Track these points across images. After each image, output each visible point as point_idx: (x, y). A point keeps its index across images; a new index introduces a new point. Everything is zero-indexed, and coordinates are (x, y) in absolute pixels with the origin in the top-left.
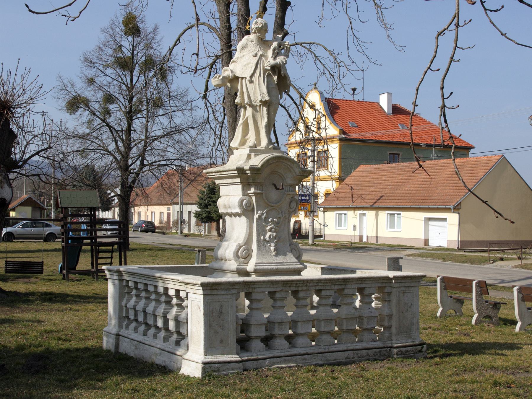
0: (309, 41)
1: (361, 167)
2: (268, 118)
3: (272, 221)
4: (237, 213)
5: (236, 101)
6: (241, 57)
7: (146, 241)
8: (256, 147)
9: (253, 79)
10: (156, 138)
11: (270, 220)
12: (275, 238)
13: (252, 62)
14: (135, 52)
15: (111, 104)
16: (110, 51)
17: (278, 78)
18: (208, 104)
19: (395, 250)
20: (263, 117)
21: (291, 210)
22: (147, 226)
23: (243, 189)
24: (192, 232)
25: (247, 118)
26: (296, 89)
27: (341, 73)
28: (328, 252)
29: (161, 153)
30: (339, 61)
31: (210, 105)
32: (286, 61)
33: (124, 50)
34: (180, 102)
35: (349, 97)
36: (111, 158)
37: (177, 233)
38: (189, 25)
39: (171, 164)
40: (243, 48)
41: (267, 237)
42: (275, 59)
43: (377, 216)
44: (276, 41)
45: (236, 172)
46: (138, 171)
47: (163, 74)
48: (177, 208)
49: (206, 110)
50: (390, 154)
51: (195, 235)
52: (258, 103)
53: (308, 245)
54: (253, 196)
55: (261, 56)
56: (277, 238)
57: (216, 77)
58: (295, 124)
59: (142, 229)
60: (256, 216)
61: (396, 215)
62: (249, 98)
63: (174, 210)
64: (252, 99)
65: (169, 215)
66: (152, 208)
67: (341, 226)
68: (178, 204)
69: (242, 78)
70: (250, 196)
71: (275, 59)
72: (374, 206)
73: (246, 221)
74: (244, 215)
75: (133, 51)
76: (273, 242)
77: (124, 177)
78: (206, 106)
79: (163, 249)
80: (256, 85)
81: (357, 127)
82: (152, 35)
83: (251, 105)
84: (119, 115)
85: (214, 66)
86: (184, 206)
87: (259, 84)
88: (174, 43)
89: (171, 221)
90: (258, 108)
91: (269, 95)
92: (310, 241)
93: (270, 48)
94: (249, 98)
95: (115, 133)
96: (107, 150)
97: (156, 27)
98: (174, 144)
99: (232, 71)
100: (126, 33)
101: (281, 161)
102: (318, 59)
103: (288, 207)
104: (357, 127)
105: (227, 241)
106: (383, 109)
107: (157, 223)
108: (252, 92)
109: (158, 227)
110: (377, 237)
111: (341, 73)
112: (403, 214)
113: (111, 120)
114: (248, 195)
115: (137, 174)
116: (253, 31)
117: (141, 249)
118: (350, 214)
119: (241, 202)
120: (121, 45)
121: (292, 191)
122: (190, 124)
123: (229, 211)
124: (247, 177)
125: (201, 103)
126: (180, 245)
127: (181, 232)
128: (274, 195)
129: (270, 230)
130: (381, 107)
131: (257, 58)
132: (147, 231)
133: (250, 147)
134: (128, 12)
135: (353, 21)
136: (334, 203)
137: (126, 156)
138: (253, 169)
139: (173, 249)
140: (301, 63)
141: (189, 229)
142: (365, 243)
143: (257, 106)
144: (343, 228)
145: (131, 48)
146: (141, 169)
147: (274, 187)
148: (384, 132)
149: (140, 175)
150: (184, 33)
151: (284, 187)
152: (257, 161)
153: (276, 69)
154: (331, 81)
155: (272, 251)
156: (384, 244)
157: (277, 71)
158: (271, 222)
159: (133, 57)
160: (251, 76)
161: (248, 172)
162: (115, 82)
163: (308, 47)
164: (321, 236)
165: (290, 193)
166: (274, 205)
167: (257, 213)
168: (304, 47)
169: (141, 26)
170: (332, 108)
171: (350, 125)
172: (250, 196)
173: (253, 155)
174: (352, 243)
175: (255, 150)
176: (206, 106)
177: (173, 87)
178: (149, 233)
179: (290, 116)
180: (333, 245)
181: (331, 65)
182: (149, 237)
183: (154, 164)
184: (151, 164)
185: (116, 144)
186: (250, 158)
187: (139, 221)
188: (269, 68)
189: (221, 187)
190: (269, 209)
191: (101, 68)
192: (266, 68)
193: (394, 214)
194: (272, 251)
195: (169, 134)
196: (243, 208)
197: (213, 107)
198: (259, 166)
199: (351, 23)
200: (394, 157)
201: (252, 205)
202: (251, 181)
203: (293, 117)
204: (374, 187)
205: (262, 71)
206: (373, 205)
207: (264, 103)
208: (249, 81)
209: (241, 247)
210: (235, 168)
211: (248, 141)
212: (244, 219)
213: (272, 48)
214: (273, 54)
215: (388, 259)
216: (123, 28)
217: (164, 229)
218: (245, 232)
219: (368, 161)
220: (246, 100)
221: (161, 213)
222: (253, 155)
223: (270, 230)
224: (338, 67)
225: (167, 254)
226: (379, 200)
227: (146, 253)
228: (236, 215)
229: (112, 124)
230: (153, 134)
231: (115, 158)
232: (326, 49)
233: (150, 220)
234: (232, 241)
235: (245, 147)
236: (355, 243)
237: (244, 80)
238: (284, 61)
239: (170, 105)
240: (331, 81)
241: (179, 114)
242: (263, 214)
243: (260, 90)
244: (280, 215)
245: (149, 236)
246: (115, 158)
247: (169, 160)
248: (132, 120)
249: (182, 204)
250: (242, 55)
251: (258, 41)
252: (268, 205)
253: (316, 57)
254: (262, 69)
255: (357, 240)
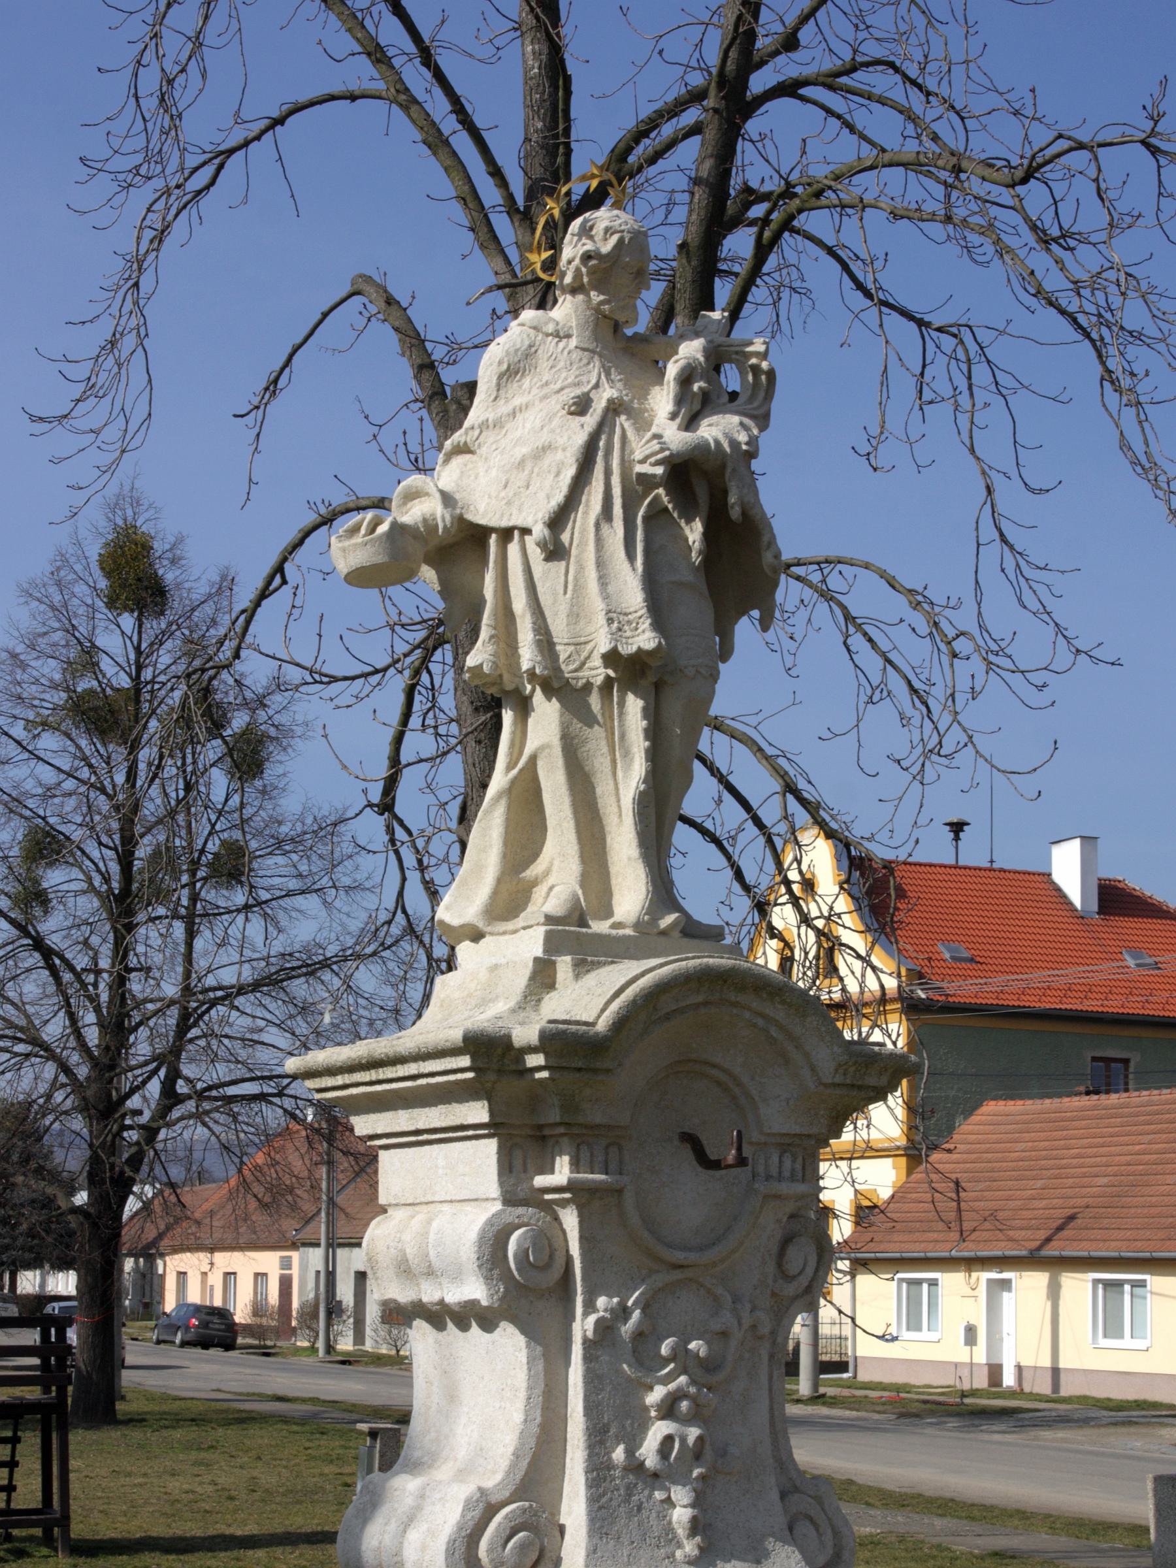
0: (821, 553)
1: (991, 1108)
2: (654, 755)
3: (680, 1355)
4: (473, 1303)
5: (471, 661)
6: (498, 424)
7: (192, 1384)
8: (583, 923)
9: (565, 537)
10: (230, 994)
11: (665, 1350)
12: (697, 1453)
13: (561, 441)
14: (147, 674)
15: (50, 865)
16: (52, 670)
17: (707, 535)
18: (400, 834)
19: (1129, 1423)
20: (627, 754)
21: (791, 1289)
22: (205, 1325)
23: (507, 1167)
24: (369, 1346)
25: (533, 759)
26: (767, 758)
27: (963, 684)
28: (875, 1428)
29: (243, 1054)
30: (951, 633)
31: (405, 838)
32: (753, 441)
33: (106, 665)
34: (314, 858)
35: (936, 848)
36: (50, 1070)
37: (313, 1349)
38: (323, 511)
39: (280, 1094)
40: (511, 373)
41: (649, 1450)
42: (690, 424)
43: (1054, 1293)
44: (697, 335)
45: (465, 1061)
46: (152, 1119)
47: (248, 759)
48: (316, 1256)
49: (392, 855)
50: (1094, 1059)
51: (378, 1360)
52: (598, 672)
53: (798, 1401)
54: (563, 1203)
55: (614, 409)
56: (708, 1453)
57: (355, 530)
58: (762, 908)
59: (189, 1337)
60: (583, 1326)
61: (1127, 1288)
62: (546, 643)
63: (304, 1268)
64: (563, 652)
65: (285, 1284)
66: (225, 1260)
67: (919, 1329)
68: (318, 1245)
69: (506, 534)
70: (548, 1207)
71: (690, 424)
72: (1045, 1252)
73: (523, 1356)
74: (515, 1321)
75: (140, 667)
76: (683, 1480)
77: (96, 1143)
78: (393, 841)
79: (245, 1419)
80: (581, 568)
81: (972, 960)
82: (209, 609)
83: (555, 684)
84: (88, 905)
85: (425, 678)
86: (340, 1252)
87: (600, 564)
88: (260, 584)
89: (295, 1304)
90: (595, 701)
91: (659, 625)
92: (804, 1386)
93: (660, 376)
94: (546, 643)
95: (67, 977)
96: (36, 1042)
97: (223, 578)
98: (291, 1017)
99: (447, 499)
100: (111, 604)
101: (733, 996)
102: (859, 627)
103: (771, 1268)
104: (972, 960)
105: (414, 1468)
106: (1064, 896)
107: (241, 1315)
108: (563, 607)
109: (248, 1329)
110: (1056, 1371)
111: (963, 684)
112: (1155, 1282)
113: (52, 926)
114: (536, 1199)
115: (150, 1133)
116: (568, 279)
117: (163, 1415)
118: (951, 1282)
119: (493, 1245)
120: (93, 646)
121: (793, 1178)
122: (350, 942)
123: (429, 1294)
124: (529, 1094)
125: (372, 827)
126: (314, 1400)
127: (330, 1349)
128: (688, 1198)
129: (668, 1410)
130: (1058, 889)
131: (591, 420)
132: (204, 1343)
133: (550, 919)
134: (120, 522)
135: (998, 481)
136: (884, 1241)
137: (109, 1061)
138: (562, 1042)
139: (284, 1419)
140: (792, 645)
141: (359, 1337)
142: (1012, 1394)
143: (588, 686)
144: (925, 1334)
145: (132, 656)
146: (168, 1109)
147: (687, 1153)
148: (1072, 974)
149: (162, 1135)
150: (301, 542)
151: (747, 1152)
152: (587, 1000)
153: (696, 480)
154: (916, 721)
155: (681, 1532)
156: (1086, 1397)
157: (702, 493)
158: (673, 1358)
159: (138, 691)
160: (558, 520)
161: (534, 1060)
162: (70, 784)
163: (816, 578)
164: (841, 1366)
165: (785, 1188)
166: (693, 1257)
167: (590, 1307)
168: (798, 578)
169: (170, 577)
170: (878, 889)
171: (947, 956)
172: (548, 1207)
173: (564, 965)
174: (963, 1395)
175: (576, 938)
176: (393, 841)
177: (290, 805)
178: (212, 1352)
179: (739, 875)
180: (891, 1402)
181: (915, 651)
182: (207, 1368)
183: (214, 1093)
184: (200, 1095)
185: (72, 1017)
186: (551, 986)
187: (182, 1305)
188: (659, 470)
189: (382, 1154)
190: (661, 1279)
191: (18, 731)
192: (639, 469)
193: (1119, 1284)
194: (681, 1532)
195: (270, 982)
196: (506, 1275)
197: (420, 843)
198: (602, 1026)
199: (989, 490)
200: (1108, 1069)
201: (560, 1262)
202: (554, 1116)
203: (750, 878)
204: (1040, 1183)
205: (617, 491)
206: (1039, 1248)
207: (630, 670)
208: (542, 545)
209: (491, 1510)
210: (455, 1035)
211: (539, 893)
212: (508, 1347)
213: (672, 370)
214: (679, 401)
215: (1158, 1480)
216: (103, 583)
217: (266, 1337)
218: (518, 1417)
219: (1012, 1086)
220: (528, 656)
221: (260, 1277)
222: (564, 965)
223: (668, 1410)
224: (945, 659)
225: (259, 1437)
226: (1060, 1229)
227: (178, 1434)
228: (464, 1316)
229: (55, 941)
230: (210, 981)
231: (65, 1068)
232: (892, 584)
233: (218, 1303)
234: (443, 1472)
235: (520, 922)
236: (974, 1393)
237: (513, 549)
238: (742, 437)
239: (273, 871)
240: (916, 721)
241: (311, 903)
242: (623, 1313)
243: (606, 597)
244: (726, 1319)
245: (208, 1361)
246: (65, 1068)
247: (270, 1078)
248: (130, 928)
249: (333, 1244)
250: (503, 408)
251: (596, 336)
252: (660, 1260)
253: (848, 618)
254: (616, 481)
255: (981, 1382)
